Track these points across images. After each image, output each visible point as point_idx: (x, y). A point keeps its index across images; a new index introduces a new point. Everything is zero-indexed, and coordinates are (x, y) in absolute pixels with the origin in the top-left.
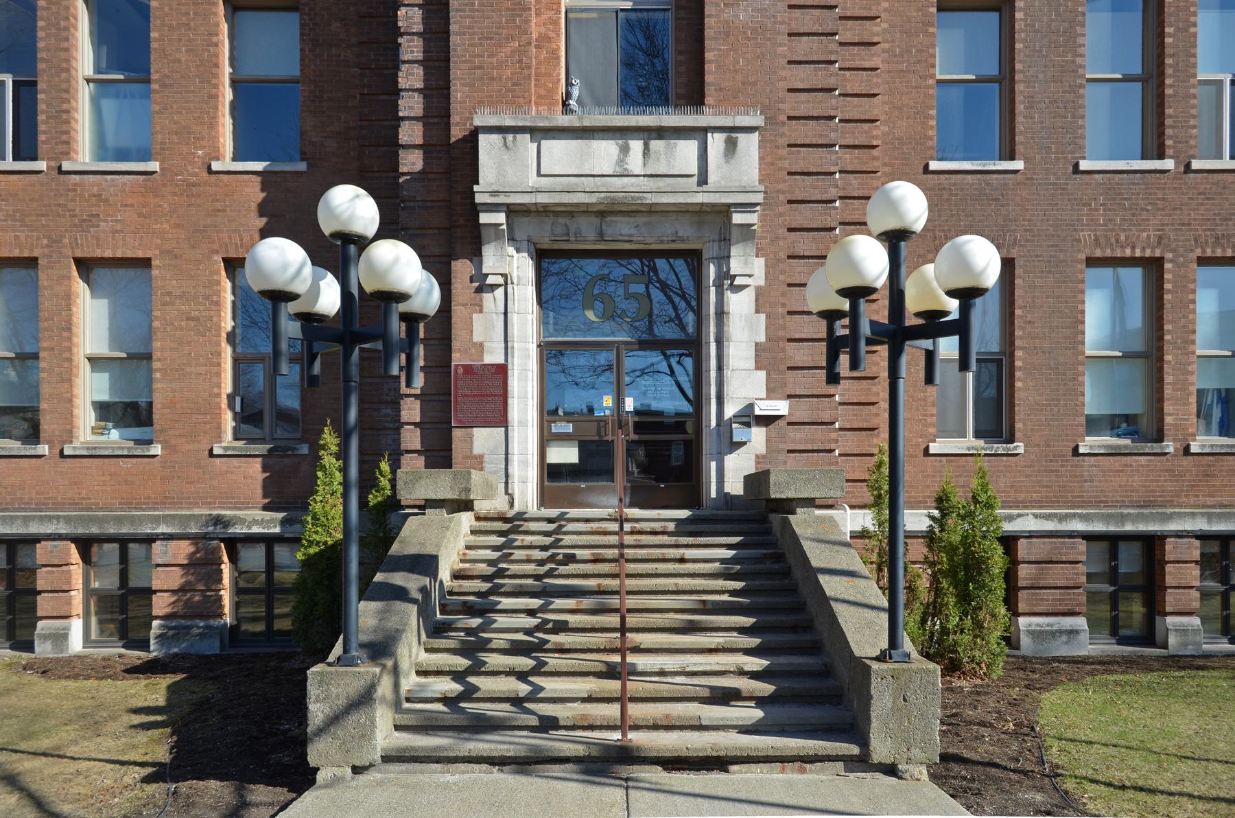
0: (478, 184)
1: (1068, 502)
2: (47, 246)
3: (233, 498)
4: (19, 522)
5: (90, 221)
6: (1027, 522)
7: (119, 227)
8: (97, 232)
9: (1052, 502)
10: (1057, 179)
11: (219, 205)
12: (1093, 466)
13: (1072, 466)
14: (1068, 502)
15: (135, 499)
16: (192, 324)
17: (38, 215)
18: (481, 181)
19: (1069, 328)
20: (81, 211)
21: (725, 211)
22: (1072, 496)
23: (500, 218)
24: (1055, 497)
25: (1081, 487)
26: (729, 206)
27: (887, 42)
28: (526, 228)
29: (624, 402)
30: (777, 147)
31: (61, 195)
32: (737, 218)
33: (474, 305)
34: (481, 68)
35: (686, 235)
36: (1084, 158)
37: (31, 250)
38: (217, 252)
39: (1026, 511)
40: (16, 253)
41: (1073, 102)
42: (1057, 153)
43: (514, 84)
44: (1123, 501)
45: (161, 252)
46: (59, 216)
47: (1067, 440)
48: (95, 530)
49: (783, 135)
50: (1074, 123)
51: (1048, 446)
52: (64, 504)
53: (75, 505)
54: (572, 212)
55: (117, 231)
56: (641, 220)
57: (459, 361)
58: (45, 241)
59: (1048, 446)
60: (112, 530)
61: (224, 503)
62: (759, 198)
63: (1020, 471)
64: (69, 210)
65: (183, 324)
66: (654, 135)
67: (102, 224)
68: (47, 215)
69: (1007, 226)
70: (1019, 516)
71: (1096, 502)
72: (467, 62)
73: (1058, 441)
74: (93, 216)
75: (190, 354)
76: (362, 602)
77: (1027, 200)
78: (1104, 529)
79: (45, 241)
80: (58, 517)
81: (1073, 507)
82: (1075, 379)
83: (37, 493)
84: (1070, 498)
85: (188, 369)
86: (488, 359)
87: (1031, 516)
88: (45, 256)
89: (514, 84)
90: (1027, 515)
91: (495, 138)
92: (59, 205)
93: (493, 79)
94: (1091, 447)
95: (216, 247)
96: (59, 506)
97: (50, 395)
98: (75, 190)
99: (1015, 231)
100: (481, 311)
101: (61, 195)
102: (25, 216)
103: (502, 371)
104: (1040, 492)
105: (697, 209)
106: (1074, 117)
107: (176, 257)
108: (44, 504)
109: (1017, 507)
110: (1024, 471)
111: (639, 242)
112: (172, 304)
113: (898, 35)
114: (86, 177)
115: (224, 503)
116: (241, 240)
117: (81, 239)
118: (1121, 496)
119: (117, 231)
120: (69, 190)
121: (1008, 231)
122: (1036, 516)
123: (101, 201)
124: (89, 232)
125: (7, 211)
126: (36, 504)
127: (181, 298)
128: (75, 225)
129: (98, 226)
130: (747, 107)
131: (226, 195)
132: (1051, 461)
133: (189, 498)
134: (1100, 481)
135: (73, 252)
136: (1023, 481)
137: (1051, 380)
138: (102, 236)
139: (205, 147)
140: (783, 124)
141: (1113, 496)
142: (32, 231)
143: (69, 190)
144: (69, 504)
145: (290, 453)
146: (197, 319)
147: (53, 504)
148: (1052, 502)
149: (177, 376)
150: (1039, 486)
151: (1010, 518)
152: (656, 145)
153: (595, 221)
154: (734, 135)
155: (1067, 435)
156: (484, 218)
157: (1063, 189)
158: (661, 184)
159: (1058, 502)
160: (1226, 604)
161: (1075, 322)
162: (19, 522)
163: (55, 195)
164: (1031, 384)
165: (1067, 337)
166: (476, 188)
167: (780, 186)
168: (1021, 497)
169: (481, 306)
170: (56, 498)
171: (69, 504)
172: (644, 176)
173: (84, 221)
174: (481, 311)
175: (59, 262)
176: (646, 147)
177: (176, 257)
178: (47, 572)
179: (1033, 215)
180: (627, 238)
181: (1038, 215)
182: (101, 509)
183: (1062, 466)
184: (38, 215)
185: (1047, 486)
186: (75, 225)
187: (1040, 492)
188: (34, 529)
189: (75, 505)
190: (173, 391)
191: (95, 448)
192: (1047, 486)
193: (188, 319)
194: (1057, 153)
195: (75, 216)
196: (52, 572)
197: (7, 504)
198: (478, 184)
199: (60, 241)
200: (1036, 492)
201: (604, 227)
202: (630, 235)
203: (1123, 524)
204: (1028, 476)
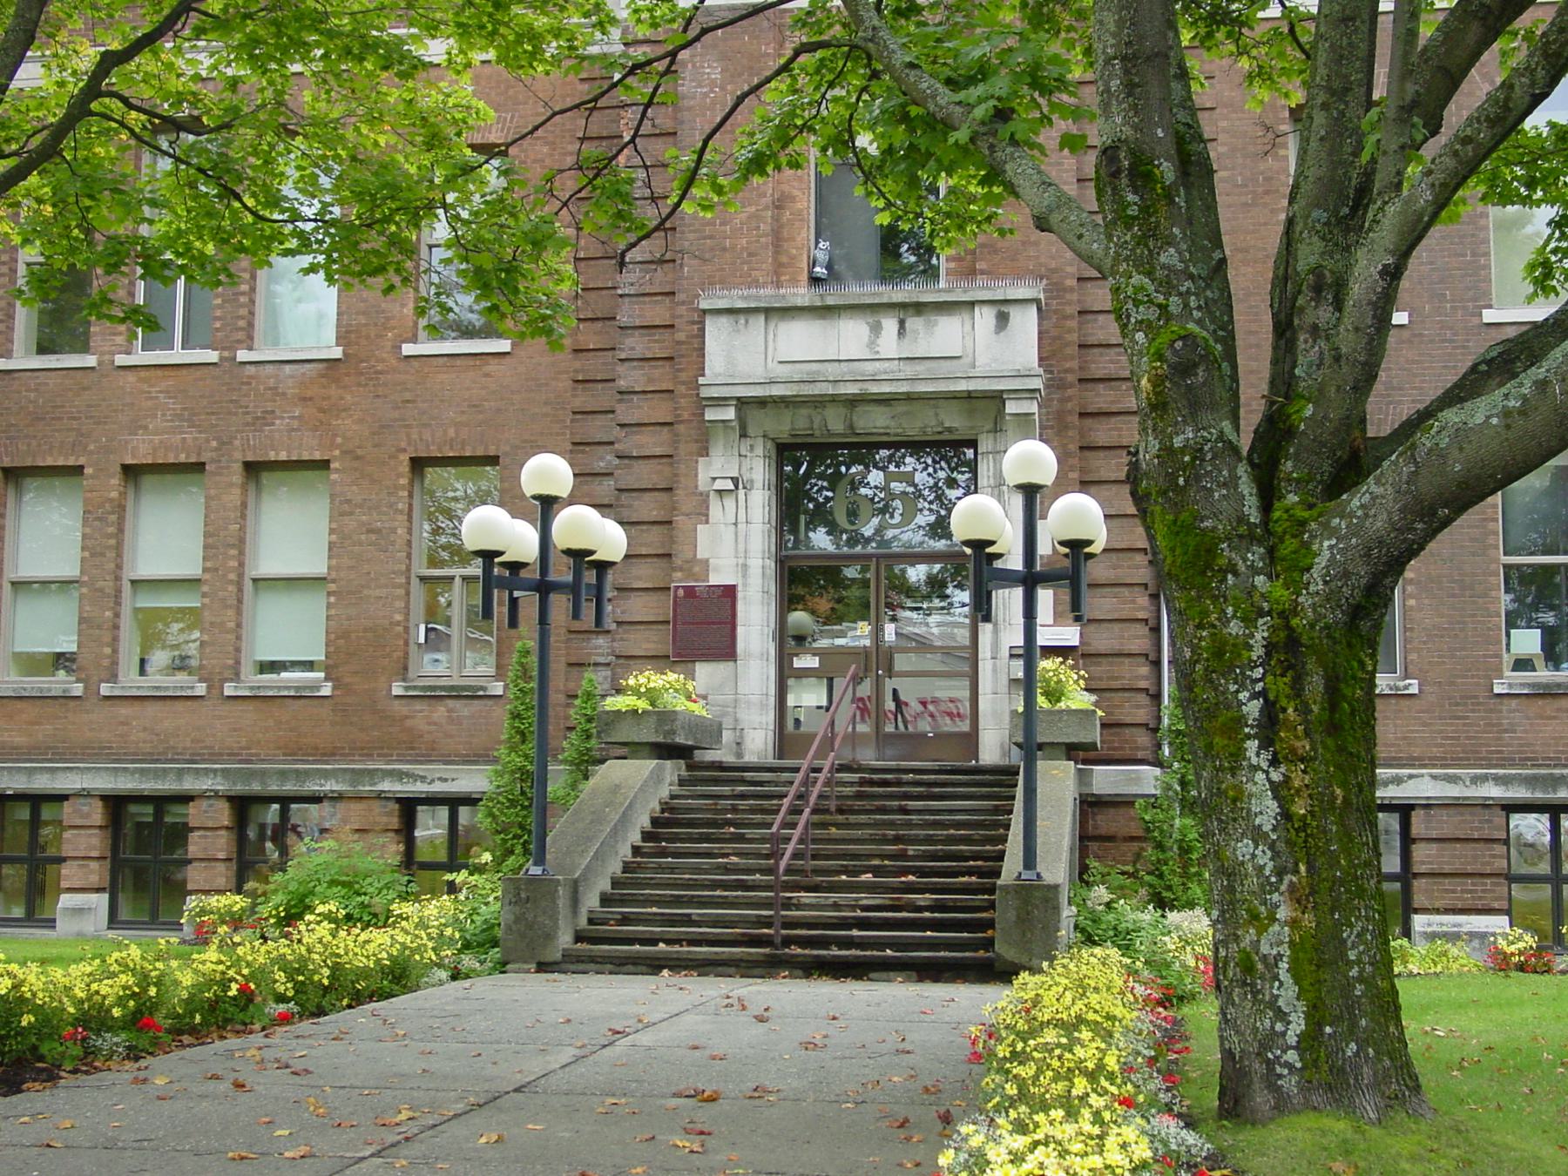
0: (703, 375)
1: (1481, 759)
2: (216, 449)
3: (412, 748)
4: (172, 776)
5: (264, 418)
6: (1421, 786)
7: (295, 424)
8: (271, 431)
9: (1461, 759)
10: (1455, 335)
11: (408, 396)
12: (1514, 711)
13: (1485, 711)
14: (1481, 759)
15: (301, 749)
16: (373, 537)
17: (208, 414)
18: (707, 371)
19: (1477, 527)
20: (256, 407)
21: (998, 398)
22: (1487, 752)
23: (730, 414)
24: (1463, 752)
25: (1499, 739)
26: (1002, 391)
27: (1226, 169)
28: (762, 422)
29: (883, 630)
30: (1066, 318)
31: (234, 389)
32: (1011, 407)
33: (699, 514)
34: (711, 237)
35: (955, 421)
36: (1490, 307)
37: (199, 454)
38: (405, 450)
39: (1424, 771)
40: (182, 458)
41: (1473, 235)
42: (1453, 301)
43: (750, 255)
44: (1559, 759)
45: (344, 453)
46: (230, 413)
47: (1478, 676)
48: (256, 787)
49: (1069, 303)
50: (1474, 262)
51: (1452, 684)
52: (221, 755)
53: (233, 756)
54: (819, 402)
55: (293, 430)
56: (901, 408)
57: (680, 581)
58: (214, 444)
59: (1452, 684)
60: (274, 787)
61: (404, 755)
62: (1037, 383)
63: (1415, 718)
64: (241, 407)
65: (363, 537)
66: (911, 311)
67: (278, 422)
68: (218, 413)
69: (1389, 395)
70: (1411, 777)
71: (1520, 759)
72: (694, 231)
73: (1466, 677)
74: (267, 412)
75: (369, 573)
76: (100, 804)
77: (1414, 362)
78: (1529, 795)
79: (214, 444)
80: (215, 771)
81: (1489, 767)
82: (1486, 596)
83: (192, 741)
84: (1484, 755)
85: (366, 592)
86: (714, 580)
87: (1427, 778)
88: (213, 461)
89: (750, 255)
90: (1422, 776)
91: (724, 321)
92: (231, 401)
93: (724, 249)
94: (1510, 686)
95: (403, 445)
96: (214, 757)
97: (211, 623)
98: (249, 384)
99: (1399, 402)
100: (707, 522)
101: (234, 389)
102: (195, 415)
103: (730, 592)
104: (1442, 745)
105: (965, 395)
106: (1474, 254)
107: (357, 458)
108: (199, 755)
109: (1412, 766)
110: (1420, 718)
111: (897, 435)
112: (351, 513)
113: (1240, 161)
114: (261, 368)
115: (404, 755)
116: (433, 436)
117: (254, 440)
118: (1555, 752)
119: (293, 430)
120: (243, 383)
121: (1390, 403)
122: (1434, 777)
123: (278, 394)
124: (262, 431)
125: (174, 409)
126: (191, 755)
127: (361, 506)
128: (248, 424)
129: (273, 424)
130: (1019, 275)
131: (418, 384)
132: (1457, 704)
133: (362, 749)
134: (1525, 731)
135: (244, 456)
136: (1417, 731)
137: (1454, 596)
138: (277, 435)
139: (394, 328)
140: (1072, 290)
141: (1543, 752)
142: (200, 432)
143: (243, 383)
144: (229, 755)
145: (481, 693)
146: (378, 531)
147: (210, 754)
148: (1461, 759)
149: (353, 601)
150: (1443, 738)
151: (1398, 781)
152: (914, 323)
153: (842, 411)
154: (1004, 309)
155: (1478, 669)
156: (710, 415)
157: (1464, 347)
158: (920, 369)
159: (1468, 759)
160: (1557, 894)
161: (1485, 520)
162: (172, 776)
163: (228, 390)
164: (1426, 601)
165: (1472, 540)
166: (701, 380)
167: (1068, 365)
168: (1416, 752)
169: (707, 515)
170: (212, 748)
171: (229, 755)
172: (900, 359)
173: (258, 418)
174: (707, 522)
175: (228, 467)
176: (902, 323)
177: (357, 458)
178: (200, 837)
179: (1423, 381)
180: (882, 431)
181: (1431, 382)
182: (263, 761)
183: (1473, 711)
184: (208, 414)
185: (1452, 738)
186: (248, 424)
187: (1442, 745)
188: (189, 785)
189: (233, 756)
190: (349, 618)
191: (259, 687)
192: (1452, 738)
193: (369, 531)
194: (1453, 301)
195: (248, 413)
196: (205, 837)
197: (159, 754)
198: (703, 375)
199: (230, 443)
200: (1436, 745)
201: (855, 418)
202: (887, 428)
203: (1555, 791)
204: (1425, 724)
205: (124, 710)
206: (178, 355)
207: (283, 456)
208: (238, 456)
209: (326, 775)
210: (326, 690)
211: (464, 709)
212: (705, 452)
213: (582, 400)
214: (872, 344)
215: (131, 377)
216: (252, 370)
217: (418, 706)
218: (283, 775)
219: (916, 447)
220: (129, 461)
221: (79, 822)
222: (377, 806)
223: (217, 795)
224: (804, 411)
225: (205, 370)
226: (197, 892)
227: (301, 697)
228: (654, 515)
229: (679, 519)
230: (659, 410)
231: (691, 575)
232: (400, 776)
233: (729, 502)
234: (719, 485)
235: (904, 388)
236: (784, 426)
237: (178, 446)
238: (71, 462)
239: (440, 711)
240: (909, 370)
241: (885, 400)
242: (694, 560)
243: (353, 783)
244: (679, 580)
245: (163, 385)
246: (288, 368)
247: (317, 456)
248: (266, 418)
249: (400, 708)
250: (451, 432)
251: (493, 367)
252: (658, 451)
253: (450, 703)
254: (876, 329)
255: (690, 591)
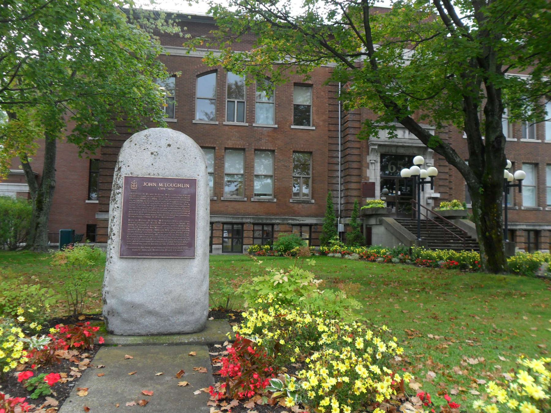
11: (292, 137)
40: (240, 147)
53: (253, 214)
86: (370, 181)
146: (286, 166)
158: (412, 141)
188: (244, 220)
189: (253, 214)
205: (227, 203)
206: (236, 123)
207: (264, 148)
208: (253, 147)
209: (276, 219)
210: (275, 200)
211: (306, 206)
212: (368, 154)
213: (330, 141)
214: (404, 135)
215: (227, 128)
216: (256, 128)
217: (295, 205)
218: (267, 219)
219: (111, 147)
220: (227, 146)
221: (217, 228)
222: (287, 226)
223: (250, 223)
224: (388, 148)
225: (245, 128)
226: (520, 236)
227: (269, 202)
228: (356, 167)
229: (364, 168)
230: (357, 145)
231: (366, 180)
232: (293, 219)
233: (373, 165)
234: (372, 161)
235: (410, 145)
236: (383, 150)
237: (240, 144)
238: (212, 146)
239: (300, 206)
240: (410, 141)
241: (403, 147)
242: (366, 177)
243: (283, 221)
244: (363, 181)
245: (234, 130)
246: (265, 129)
247: (272, 149)
248: (260, 139)
249: (292, 205)
250: (302, 146)
251: (311, 132)
252: (356, 153)
253: (303, 204)
254: (404, 132)
255: (366, 183)
